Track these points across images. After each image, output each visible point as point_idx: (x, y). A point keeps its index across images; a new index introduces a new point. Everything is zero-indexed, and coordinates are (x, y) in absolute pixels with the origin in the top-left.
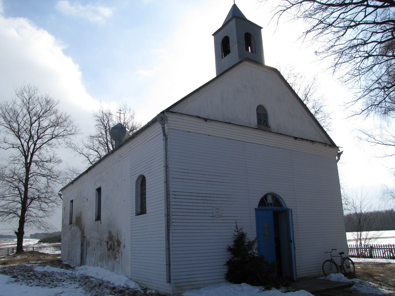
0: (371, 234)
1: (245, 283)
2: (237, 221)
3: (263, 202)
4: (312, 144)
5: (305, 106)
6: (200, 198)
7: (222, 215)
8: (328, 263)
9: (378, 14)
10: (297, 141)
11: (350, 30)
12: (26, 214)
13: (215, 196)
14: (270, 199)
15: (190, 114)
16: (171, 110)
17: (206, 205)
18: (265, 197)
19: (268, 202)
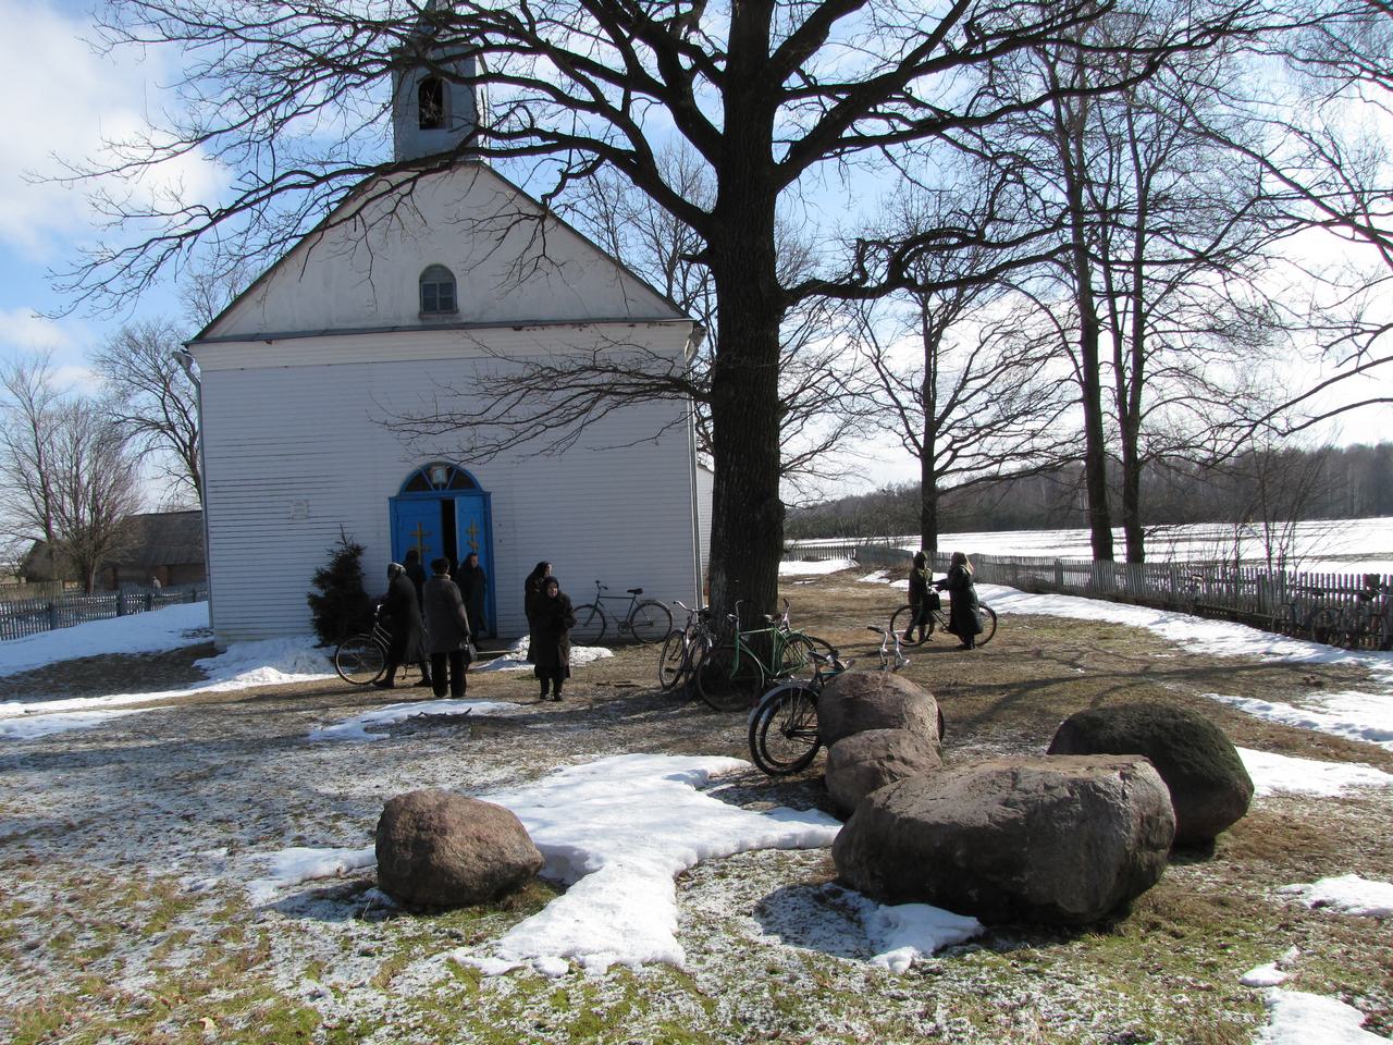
0: (805, 542)
1: (720, 179)
2: (345, 525)
3: (418, 482)
4: (577, 329)
5: (618, 263)
6: (264, 487)
7: (311, 514)
8: (589, 611)
9: (875, 65)
10: (523, 333)
11: (534, 395)
12: (712, 286)
13: (295, 480)
14: (439, 476)
15: (301, 327)
16: (209, 336)
17: (275, 498)
18: (428, 469)
19: (435, 481)
